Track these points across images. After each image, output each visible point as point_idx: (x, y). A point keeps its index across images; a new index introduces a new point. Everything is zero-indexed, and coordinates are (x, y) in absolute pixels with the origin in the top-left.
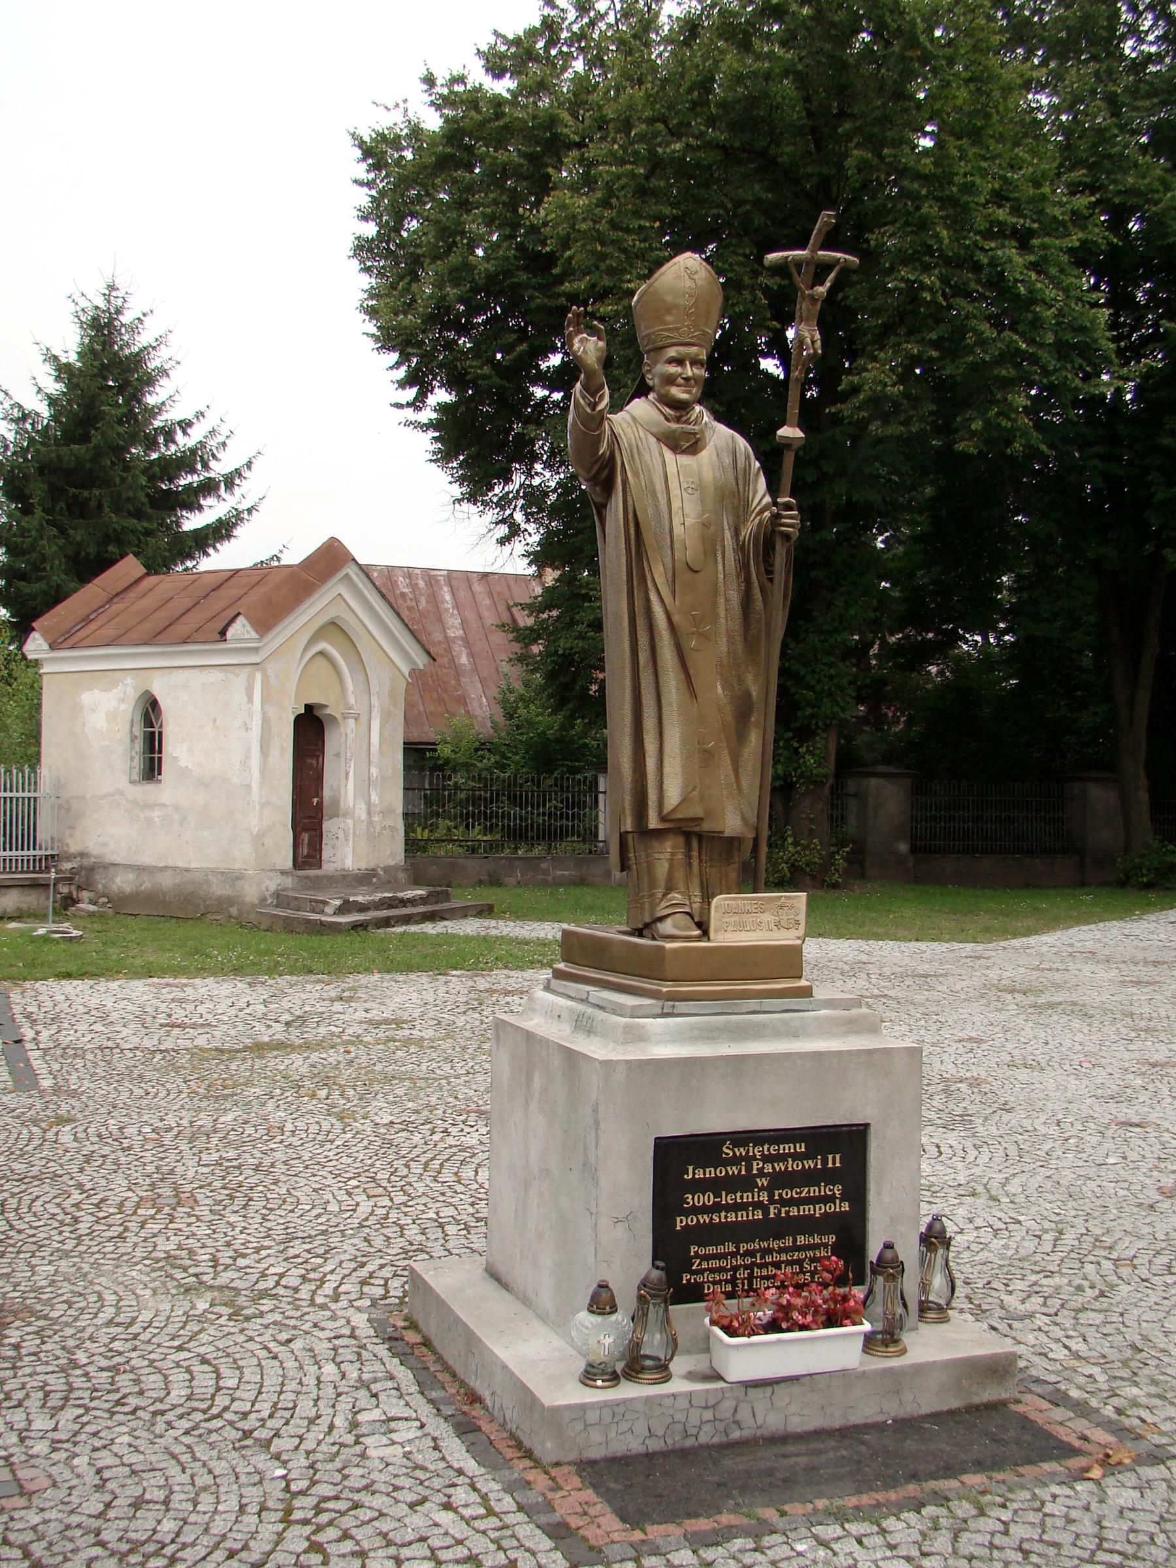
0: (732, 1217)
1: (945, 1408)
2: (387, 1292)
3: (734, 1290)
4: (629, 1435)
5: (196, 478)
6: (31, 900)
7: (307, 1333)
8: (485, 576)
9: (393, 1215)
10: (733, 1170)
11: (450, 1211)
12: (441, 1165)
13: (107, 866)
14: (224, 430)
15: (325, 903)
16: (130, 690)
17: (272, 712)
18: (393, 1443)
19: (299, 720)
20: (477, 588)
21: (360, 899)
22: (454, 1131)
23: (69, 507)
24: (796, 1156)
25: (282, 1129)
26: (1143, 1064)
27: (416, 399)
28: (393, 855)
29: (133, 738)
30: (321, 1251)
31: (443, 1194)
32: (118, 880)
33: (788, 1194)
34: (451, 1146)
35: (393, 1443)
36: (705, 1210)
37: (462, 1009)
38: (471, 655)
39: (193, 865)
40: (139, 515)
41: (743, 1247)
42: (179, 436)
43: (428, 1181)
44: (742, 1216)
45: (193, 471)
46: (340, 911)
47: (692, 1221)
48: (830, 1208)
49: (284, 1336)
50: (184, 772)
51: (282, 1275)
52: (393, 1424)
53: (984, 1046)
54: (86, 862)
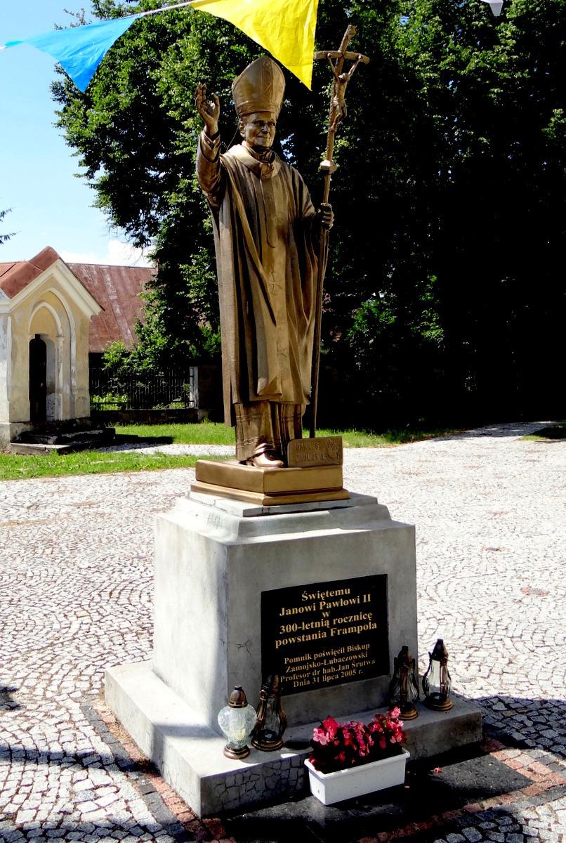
2: (91, 685)
4: (253, 791)
7: (41, 721)
8: (128, 268)
9: (93, 629)
10: (308, 609)
11: (127, 624)
12: (120, 593)
17: (17, 338)
18: (100, 808)
19: (32, 343)
20: (124, 274)
22: (125, 570)
24: (345, 597)
25: (25, 575)
26: (490, 513)
27: (89, 172)
28: (84, 411)
30: (48, 658)
31: (122, 613)
33: (341, 621)
34: (124, 581)
35: (100, 808)
36: (292, 634)
37: (125, 494)
38: (122, 308)
43: (112, 603)
44: (315, 637)
49: (25, 726)
51: (25, 678)
52: (98, 792)
53: (404, 506)
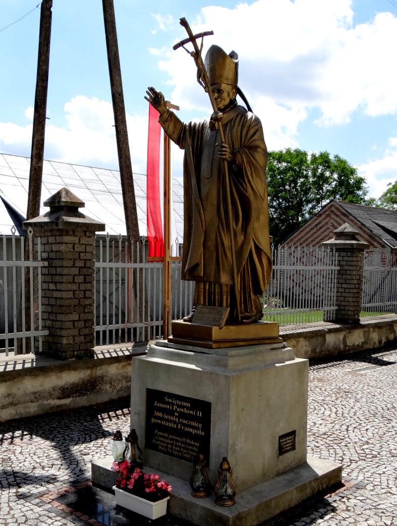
24: (188, 408)
41: (170, 436)
44: (170, 425)
47: (156, 421)
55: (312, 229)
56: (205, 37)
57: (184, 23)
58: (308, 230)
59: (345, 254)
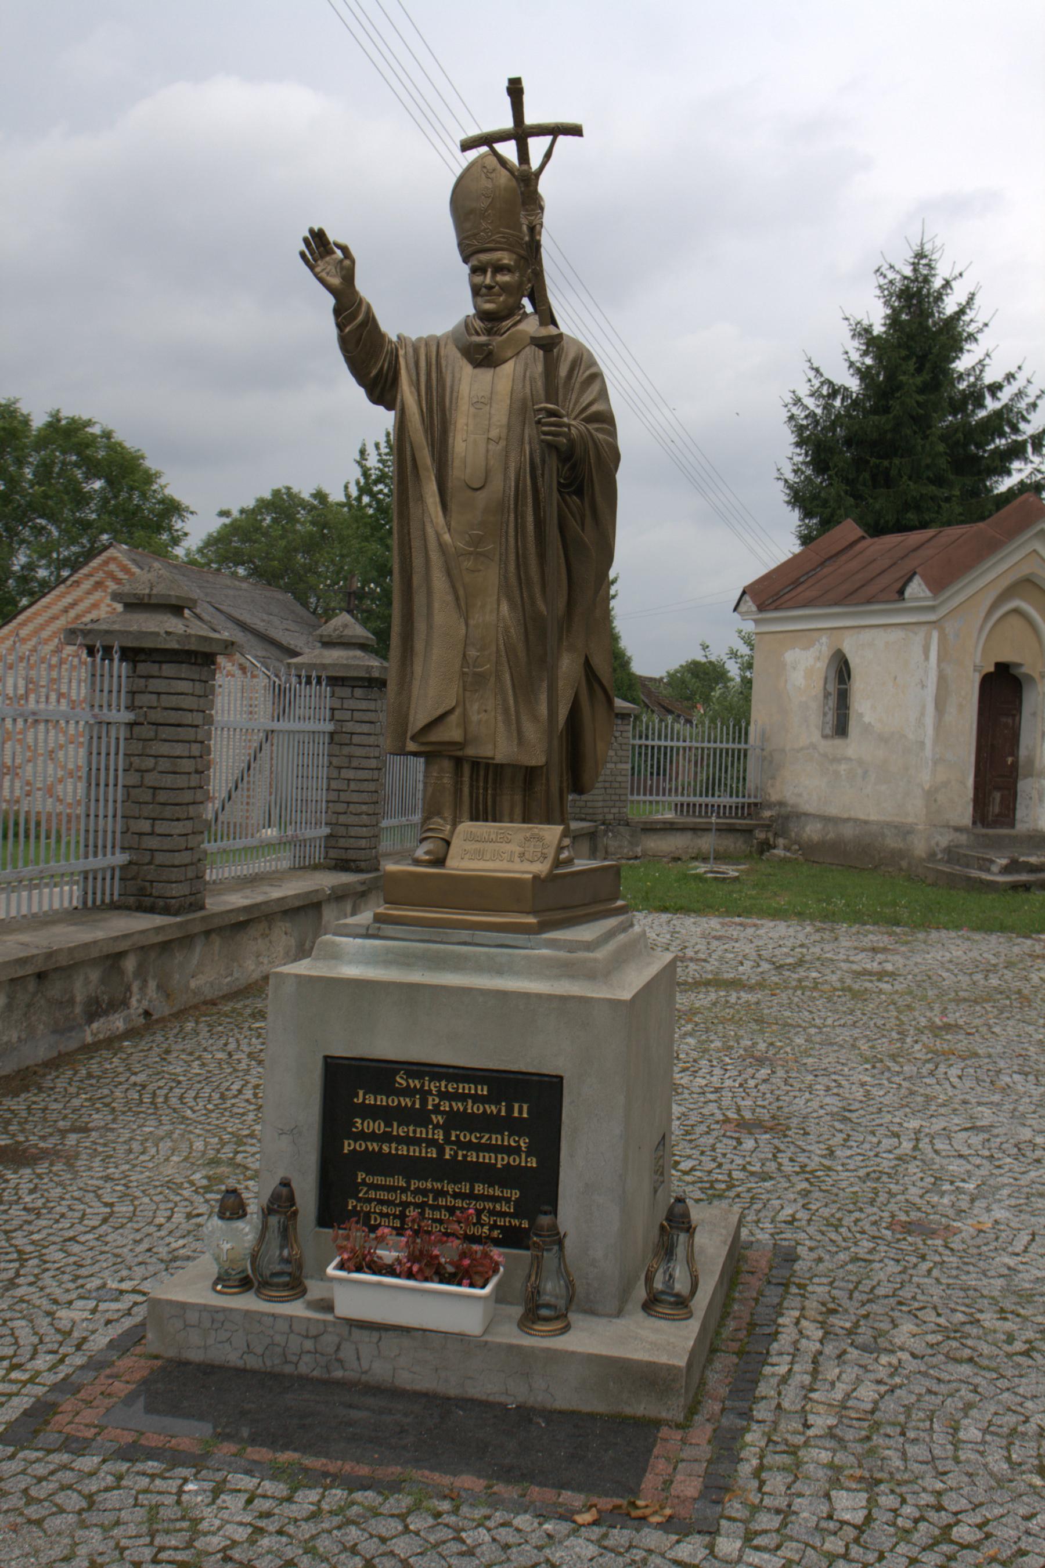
0: (403, 1150)
1: (586, 1408)
3: (402, 1228)
5: (1003, 441)
6: (729, 843)
13: (801, 816)
14: (1033, 392)
15: (992, 862)
16: (824, 648)
21: (1033, 860)
23: (874, 477)
24: (476, 1098)
29: (827, 695)
32: (808, 829)
33: (465, 1137)
36: (373, 1137)
39: (872, 818)
40: (939, 481)
41: (414, 1184)
42: (988, 401)
44: (414, 1151)
45: (1002, 435)
46: (1006, 870)
47: (360, 1146)
48: (514, 1161)
50: (867, 728)
54: (783, 811)
55: (55, 618)
56: (561, 139)
57: (515, 90)
58: (40, 620)
59: (346, 692)
